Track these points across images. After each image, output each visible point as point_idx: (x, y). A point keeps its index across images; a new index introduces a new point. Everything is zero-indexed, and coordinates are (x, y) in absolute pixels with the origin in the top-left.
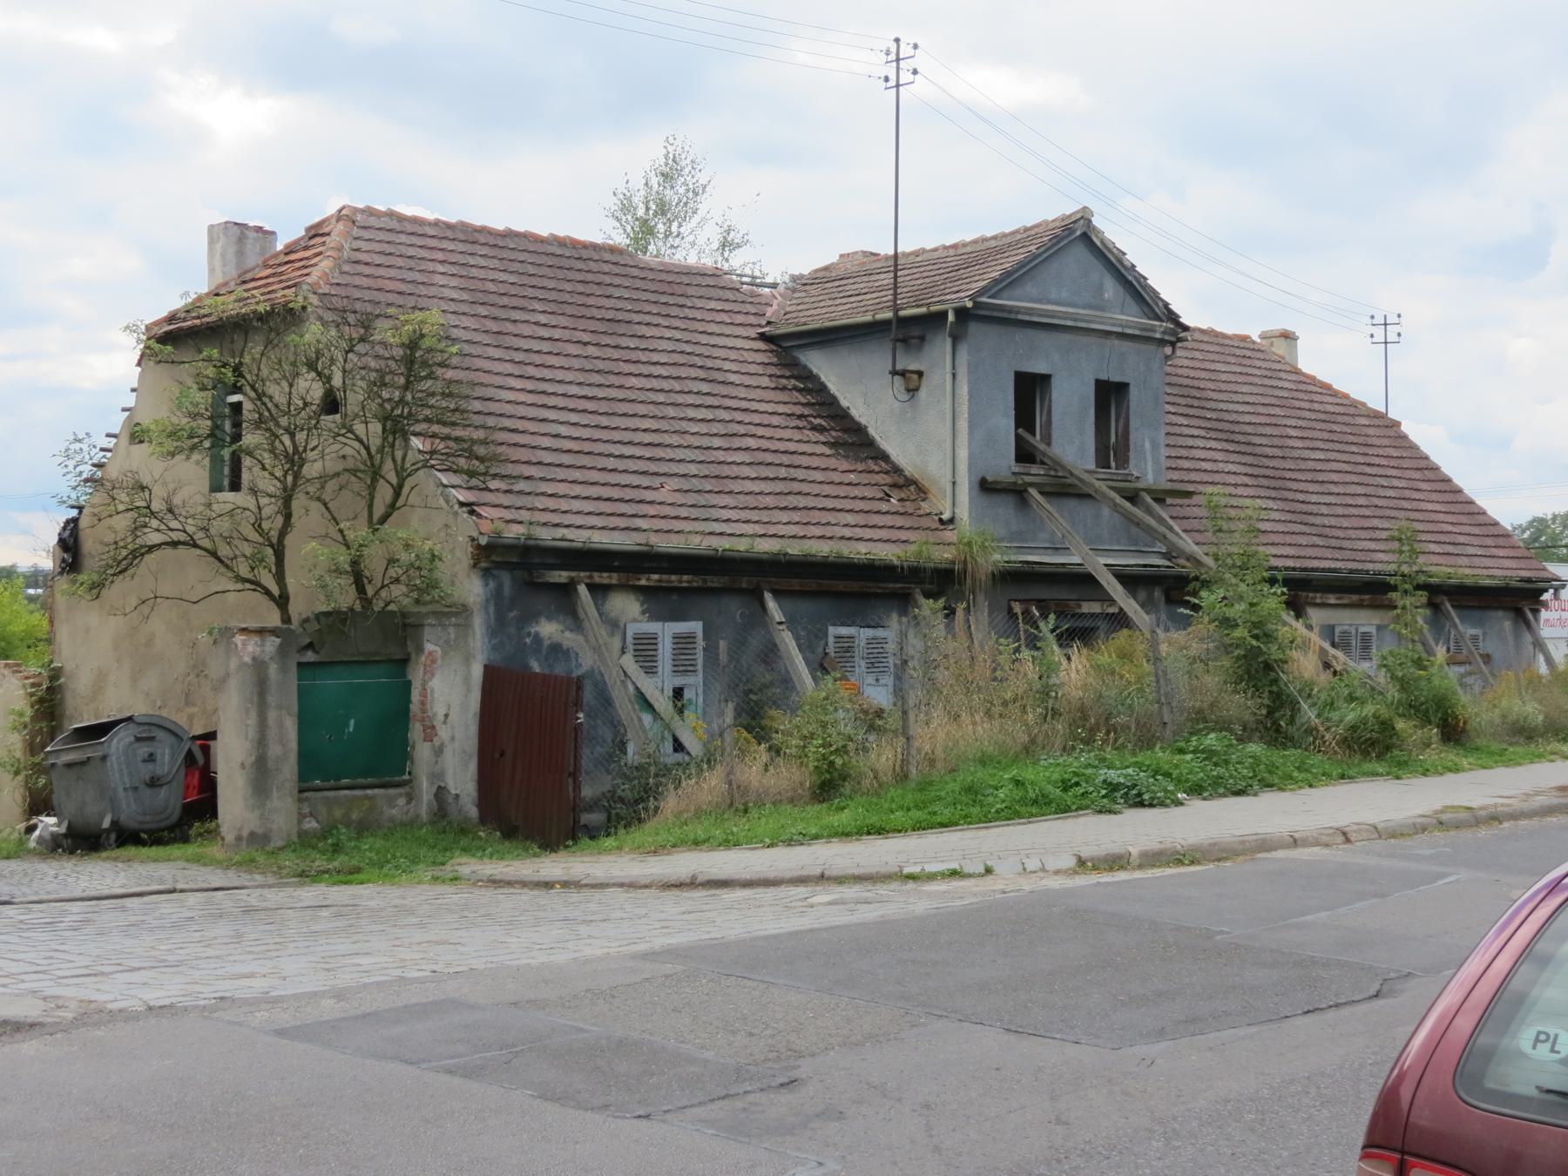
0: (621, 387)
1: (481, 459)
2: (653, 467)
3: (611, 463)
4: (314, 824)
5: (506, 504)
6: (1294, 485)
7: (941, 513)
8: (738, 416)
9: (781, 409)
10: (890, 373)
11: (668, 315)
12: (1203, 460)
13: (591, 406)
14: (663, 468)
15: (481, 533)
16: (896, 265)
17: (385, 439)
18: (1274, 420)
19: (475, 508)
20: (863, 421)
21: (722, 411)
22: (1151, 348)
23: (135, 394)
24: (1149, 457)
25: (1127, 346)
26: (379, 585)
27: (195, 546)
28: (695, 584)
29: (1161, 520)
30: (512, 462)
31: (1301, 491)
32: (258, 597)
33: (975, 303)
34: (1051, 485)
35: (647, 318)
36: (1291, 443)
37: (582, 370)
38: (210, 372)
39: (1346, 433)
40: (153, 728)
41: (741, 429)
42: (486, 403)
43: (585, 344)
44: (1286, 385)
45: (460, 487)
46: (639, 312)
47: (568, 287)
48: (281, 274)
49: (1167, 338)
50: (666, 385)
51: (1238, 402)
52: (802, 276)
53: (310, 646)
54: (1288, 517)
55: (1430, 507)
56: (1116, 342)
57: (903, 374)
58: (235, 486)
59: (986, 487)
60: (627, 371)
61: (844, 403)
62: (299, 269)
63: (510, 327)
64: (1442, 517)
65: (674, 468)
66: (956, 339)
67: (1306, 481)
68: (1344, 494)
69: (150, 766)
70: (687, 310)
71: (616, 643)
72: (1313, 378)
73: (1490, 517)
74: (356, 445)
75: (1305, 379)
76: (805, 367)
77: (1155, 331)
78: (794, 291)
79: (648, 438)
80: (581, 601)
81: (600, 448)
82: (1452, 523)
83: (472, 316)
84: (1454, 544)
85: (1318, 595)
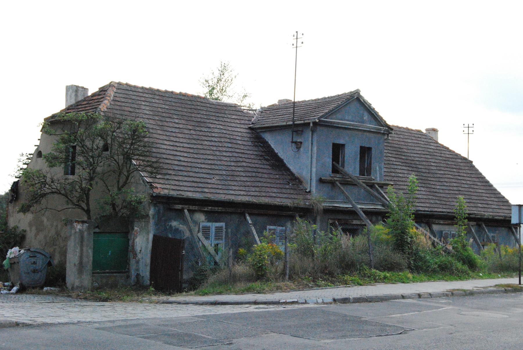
0: (201, 144)
1: (155, 168)
2: (211, 172)
3: (197, 170)
4: (97, 284)
5: (162, 183)
6: (432, 183)
7: (306, 189)
8: (240, 155)
9: (255, 153)
10: (291, 142)
11: (219, 120)
12: (399, 173)
13: (191, 151)
14: (214, 172)
15: (154, 192)
16: (294, 106)
17: (124, 161)
18: (427, 160)
19: (152, 184)
20: (282, 157)
21: (235, 153)
22: (380, 135)
23: (39, 141)
24: (378, 172)
25: (372, 135)
26: (120, 208)
27: (60, 193)
28: (223, 211)
29: (380, 194)
30: (165, 169)
31: (434, 185)
32: (79, 210)
33: (319, 120)
34: (343, 181)
35: (211, 121)
36: (432, 168)
37: (189, 139)
38: (66, 136)
39: (452, 165)
40: (36, 253)
41: (241, 160)
42: (157, 149)
43: (190, 130)
44: (432, 147)
45: (147, 177)
46: (209, 119)
47: (186, 110)
48: (90, 103)
49: (385, 132)
50: (216, 144)
51: (415, 153)
52: (265, 108)
53: (97, 227)
54: (428, 193)
55: (480, 191)
56: (368, 134)
57: (296, 143)
58: (73, 173)
59: (321, 181)
60: (204, 139)
61: (276, 151)
62: (96, 102)
63: (166, 124)
64: (484, 195)
65: (217, 172)
66: (313, 132)
67: (436, 181)
68: (450, 186)
69: (34, 266)
70: (225, 119)
71: (197, 229)
72: (442, 145)
73: (502, 195)
74: (114, 162)
75: (439, 146)
76: (264, 138)
77: (381, 130)
78: (262, 112)
79: (210, 162)
80: (185, 214)
81: (194, 165)
82: (488, 197)
83: (153, 120)
84: (487, 204)
85: (437, 220)
